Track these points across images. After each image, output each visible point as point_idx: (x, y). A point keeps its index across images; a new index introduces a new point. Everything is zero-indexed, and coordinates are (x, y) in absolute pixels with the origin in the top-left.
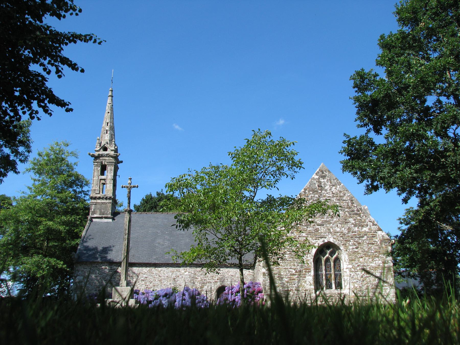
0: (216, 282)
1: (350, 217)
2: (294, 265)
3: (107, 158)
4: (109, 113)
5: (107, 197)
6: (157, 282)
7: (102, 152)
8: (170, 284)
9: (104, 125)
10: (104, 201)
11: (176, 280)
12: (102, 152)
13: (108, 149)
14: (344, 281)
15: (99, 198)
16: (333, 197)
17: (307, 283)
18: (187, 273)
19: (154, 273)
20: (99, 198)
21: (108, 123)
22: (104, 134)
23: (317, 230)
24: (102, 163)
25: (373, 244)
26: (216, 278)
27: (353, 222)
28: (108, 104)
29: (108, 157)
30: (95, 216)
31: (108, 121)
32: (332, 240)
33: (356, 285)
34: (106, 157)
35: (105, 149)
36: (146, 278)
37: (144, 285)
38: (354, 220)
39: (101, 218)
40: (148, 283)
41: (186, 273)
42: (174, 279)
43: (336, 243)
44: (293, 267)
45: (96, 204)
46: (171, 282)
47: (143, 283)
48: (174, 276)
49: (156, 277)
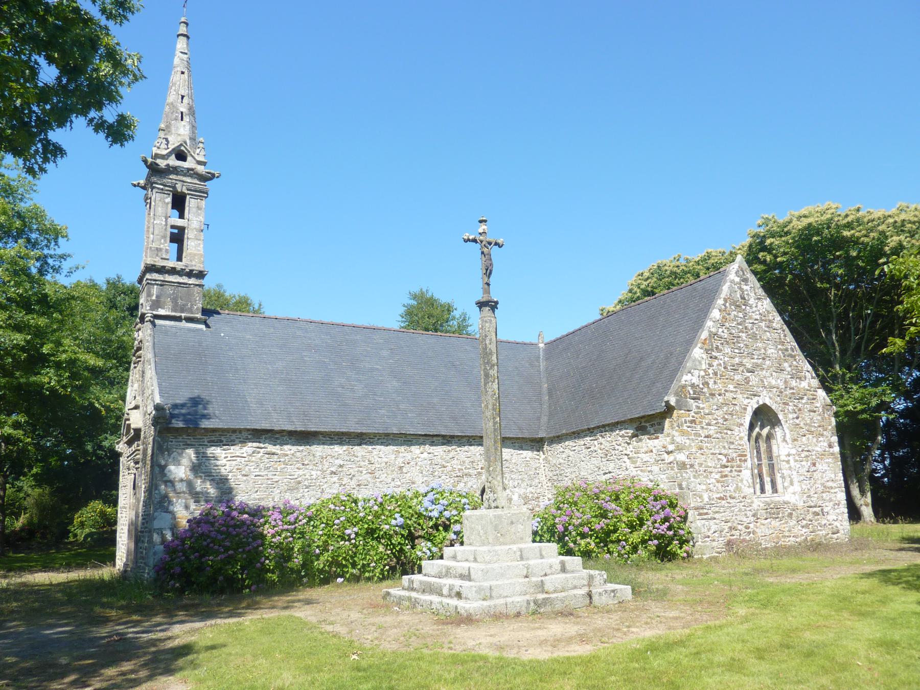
0: (479, 473)
1: (785, 361)
2: (724, 447)
3: (188, 180)
4: (183, 73)
5: (191, 271)
6: (366, 477)
7: (173, 162)
8: (393, 480)
9: (172, 97)
10: (184, 280)
11: (404, 470)
12: (173, 162)
13: (189, 158)
14: (783, 477)
15: (173, 271)
16: (762, 320)
17: (745, 482)
18: (425, 455)
19: (360, 454)
20: (173, 271)
21: (183, 97)
22: (176, 119)
23: (747, 380)
24: (174, 187)
25: (815, 412)
26: (480, 467)
27: (789, 369)
28: (178, 54)
29: (191, 176)
30: (161, 312)
31: (182, 92)
32: (768, 402)
33: (804, 487)
34: (185, 175)
35: (181, 156)
36: (341, 466)
37: (337, 485)
38: (790, 366)
39: (179, 319)
40: (345, 479)
41: (422, 456)
42: (401, 468)
43: (773, 407)
44: (723, 451)
45: (163, 284)
46: (395, 475)
47: (335, 479)
48: (400, 461)
49: (362, 464)
